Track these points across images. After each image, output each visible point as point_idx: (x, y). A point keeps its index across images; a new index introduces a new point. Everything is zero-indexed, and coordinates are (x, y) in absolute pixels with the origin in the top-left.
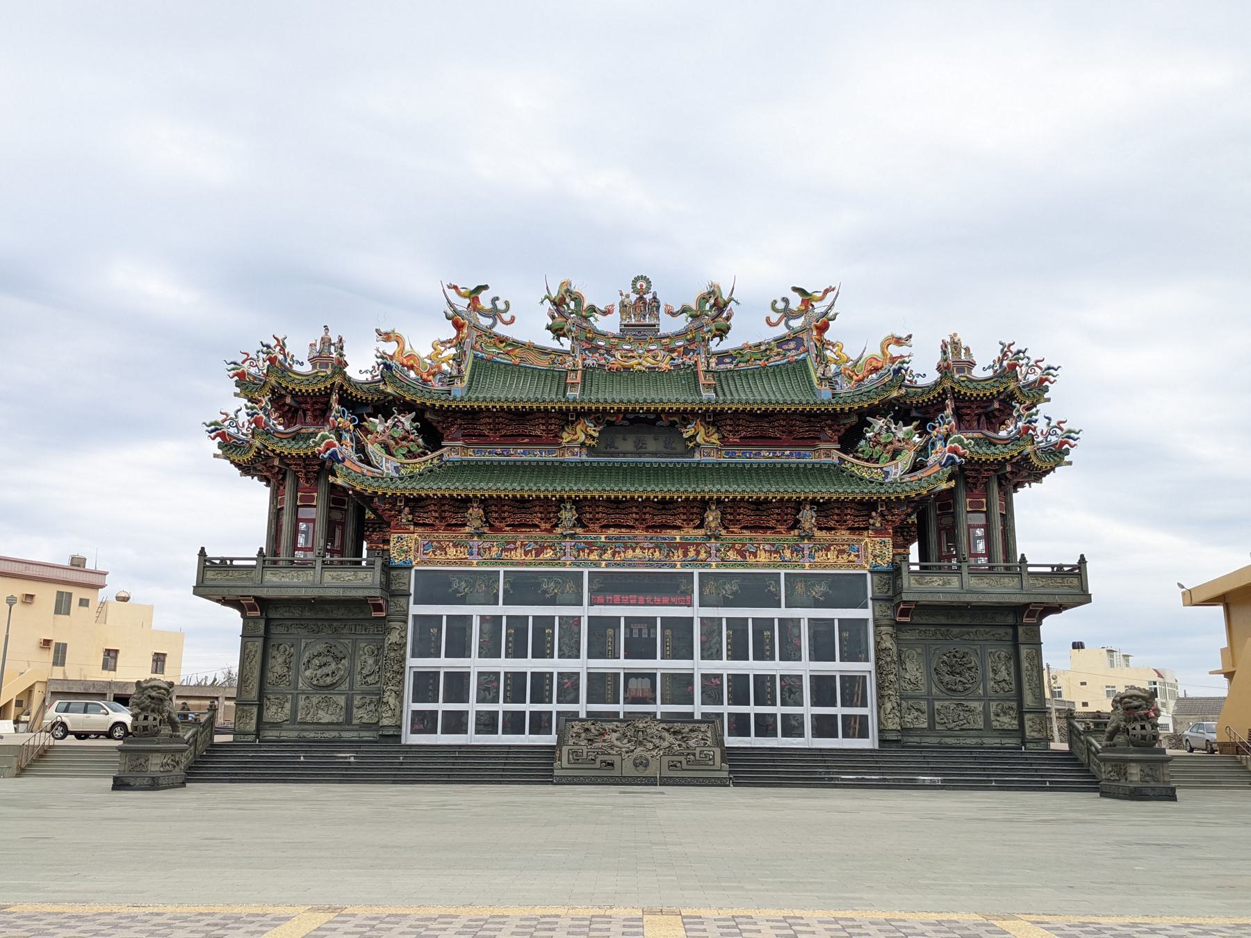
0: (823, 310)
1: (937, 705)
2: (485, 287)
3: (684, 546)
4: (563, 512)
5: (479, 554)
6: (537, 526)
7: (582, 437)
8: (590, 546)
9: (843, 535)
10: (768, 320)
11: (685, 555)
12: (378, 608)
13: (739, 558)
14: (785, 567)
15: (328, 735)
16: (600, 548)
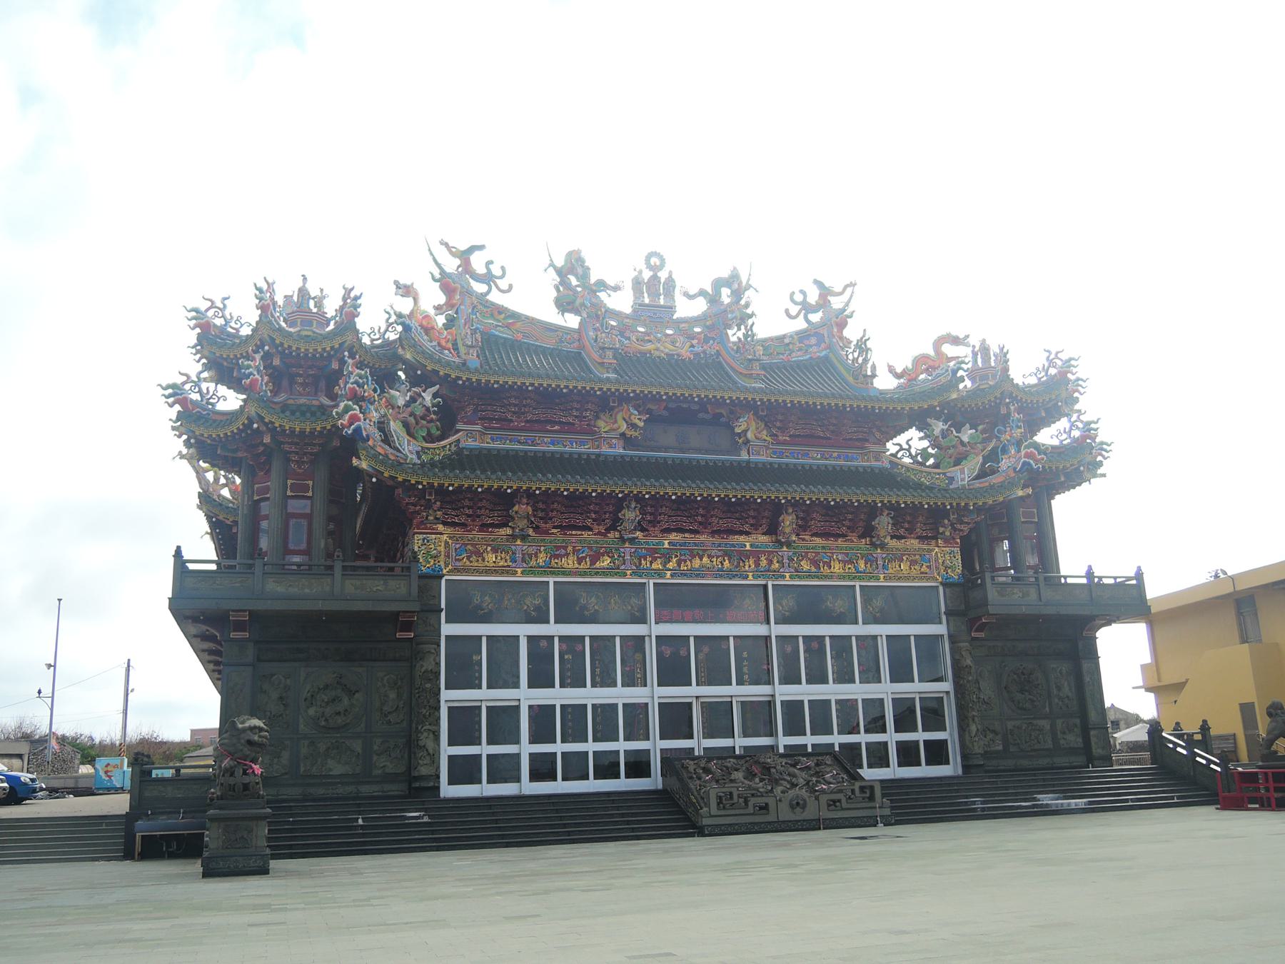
0: (841, 306)
1: (1010, 725)
2: (481, 248)
3: (756, 554)
4: (625, 511)
5: (523, 560)
6: (590, 529)
7: (624, 427)
8: (653, 553)
9: (913, 543)
10: (787, 311)
11: (757, 564)
12: (407, 626)
13: (813, 569)
14: (860, 579)
15: (341, 790)
16: (663, 555)
